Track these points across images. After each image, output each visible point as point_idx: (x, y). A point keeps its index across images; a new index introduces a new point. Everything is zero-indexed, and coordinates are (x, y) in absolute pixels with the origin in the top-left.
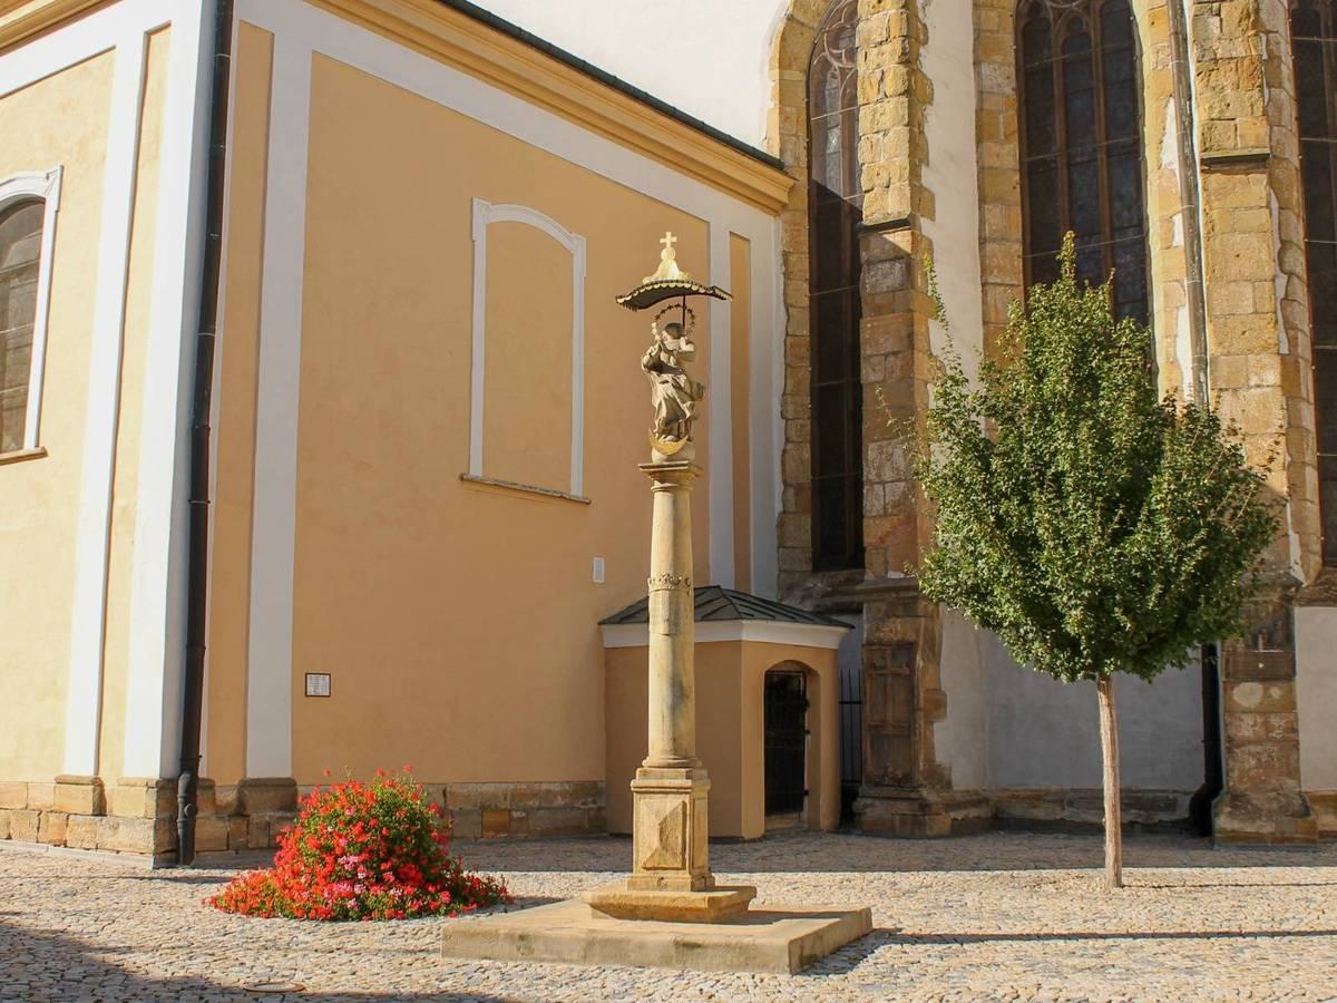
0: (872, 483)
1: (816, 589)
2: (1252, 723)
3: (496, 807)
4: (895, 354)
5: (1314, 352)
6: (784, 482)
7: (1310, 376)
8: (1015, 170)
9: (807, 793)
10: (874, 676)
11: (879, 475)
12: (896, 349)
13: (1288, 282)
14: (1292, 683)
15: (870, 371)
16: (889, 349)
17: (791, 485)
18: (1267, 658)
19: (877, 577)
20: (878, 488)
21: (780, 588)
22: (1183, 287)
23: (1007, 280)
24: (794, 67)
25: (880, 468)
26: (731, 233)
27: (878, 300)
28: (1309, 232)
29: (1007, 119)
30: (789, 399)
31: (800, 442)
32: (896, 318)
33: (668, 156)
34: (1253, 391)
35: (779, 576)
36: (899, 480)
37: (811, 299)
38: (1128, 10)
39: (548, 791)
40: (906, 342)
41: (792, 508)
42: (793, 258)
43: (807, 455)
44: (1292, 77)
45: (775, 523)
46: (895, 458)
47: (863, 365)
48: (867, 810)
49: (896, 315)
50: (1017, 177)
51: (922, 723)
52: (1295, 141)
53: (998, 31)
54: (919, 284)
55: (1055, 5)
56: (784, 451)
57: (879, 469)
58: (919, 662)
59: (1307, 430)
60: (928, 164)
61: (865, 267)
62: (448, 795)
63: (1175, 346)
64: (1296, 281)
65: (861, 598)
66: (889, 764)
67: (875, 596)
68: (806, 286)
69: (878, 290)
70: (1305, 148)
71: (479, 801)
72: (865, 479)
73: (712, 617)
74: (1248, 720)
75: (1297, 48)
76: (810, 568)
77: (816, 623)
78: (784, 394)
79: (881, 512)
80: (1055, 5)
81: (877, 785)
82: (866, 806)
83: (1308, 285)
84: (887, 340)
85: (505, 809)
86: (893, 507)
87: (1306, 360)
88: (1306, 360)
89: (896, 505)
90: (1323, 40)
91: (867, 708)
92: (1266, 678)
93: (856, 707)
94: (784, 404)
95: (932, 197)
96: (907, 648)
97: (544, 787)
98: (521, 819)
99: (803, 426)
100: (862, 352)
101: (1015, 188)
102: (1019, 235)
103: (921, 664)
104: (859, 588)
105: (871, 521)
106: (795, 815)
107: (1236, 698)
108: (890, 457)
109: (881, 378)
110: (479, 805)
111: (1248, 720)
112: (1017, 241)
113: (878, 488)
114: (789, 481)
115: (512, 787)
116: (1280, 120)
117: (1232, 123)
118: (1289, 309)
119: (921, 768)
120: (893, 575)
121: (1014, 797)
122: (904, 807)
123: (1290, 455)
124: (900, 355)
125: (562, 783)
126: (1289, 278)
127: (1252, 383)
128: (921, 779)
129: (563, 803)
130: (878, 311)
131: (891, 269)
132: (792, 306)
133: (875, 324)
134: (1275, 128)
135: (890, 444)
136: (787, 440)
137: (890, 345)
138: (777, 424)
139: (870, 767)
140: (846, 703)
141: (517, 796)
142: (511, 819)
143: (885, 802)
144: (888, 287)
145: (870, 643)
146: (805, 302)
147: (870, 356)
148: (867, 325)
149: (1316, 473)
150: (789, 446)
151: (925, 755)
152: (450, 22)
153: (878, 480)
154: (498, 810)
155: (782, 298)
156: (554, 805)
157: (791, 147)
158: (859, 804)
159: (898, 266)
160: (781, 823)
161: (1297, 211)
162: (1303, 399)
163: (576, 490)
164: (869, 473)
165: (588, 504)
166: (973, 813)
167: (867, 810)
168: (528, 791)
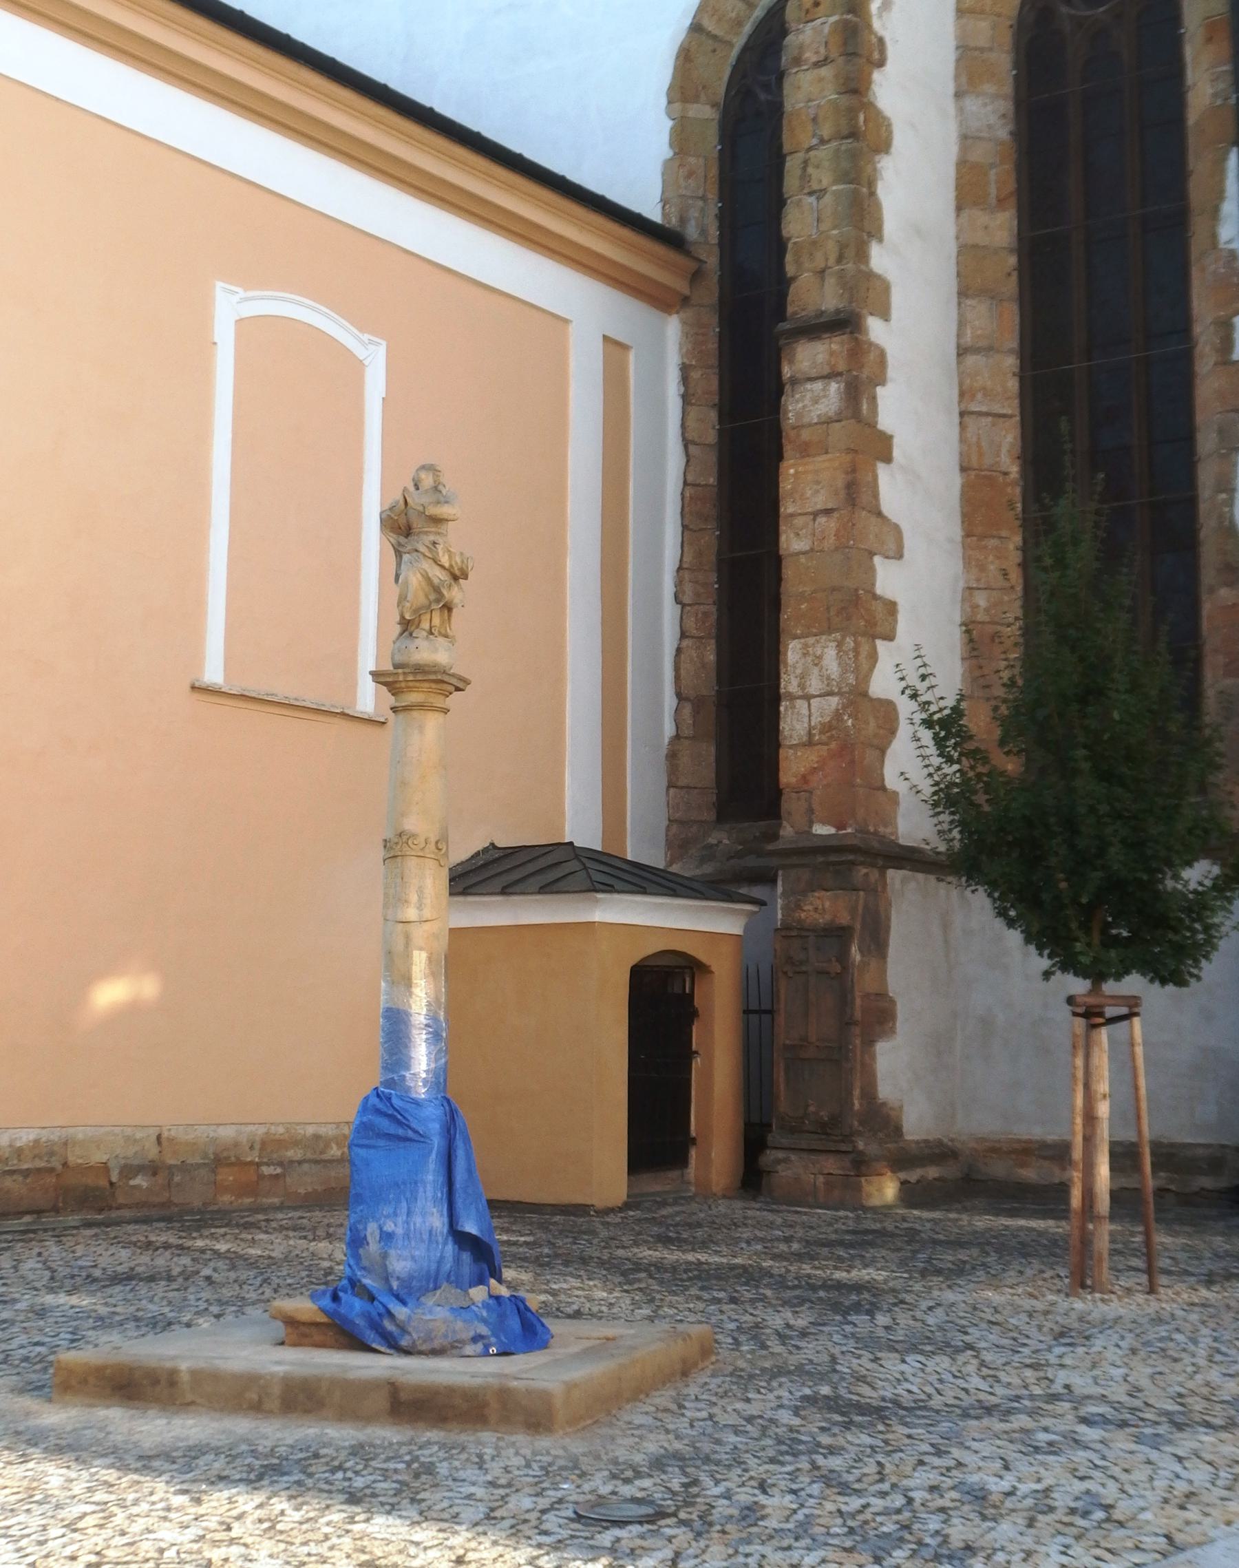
0: (792, 698)
1: (721, 847)
3: (238, 1159)
4: (827, 512)
6: (679, 695)
8: (1011, 251)
9: (693, 1141)
10: (790, 974)
11: (802, 686)
12: (829, 506)
15: (792, 535)
16: (819, 507)
17: (687, 699)
19: (797, 833)
20: (801, 705)
21: (669, 844)
23: (997, 409)
24: (703, 97)
25: (802, 677)
26: (606, 339)
27: (805, 435)
30: (687, 575)
31: (702, 638)
32: (829, 460)
33: (412, 178)
35: (668, 828)
36: (830, 694)
37: (721, 433)
38: (1175, 19)
39: (317, 1137)
40: (842, 494)
41: (687, 731)
43: (711, 657)
45: (665, 752)
46: (824, 663)
48: (779, 1168)
49: (829, 456)
50: (1013, 260)
51: (858, 1042)
53: (991, 49)
54: (865, 412)
55: (1073, 12)
56: (679, 651)
58: (855, 954)
60: (880, 240)
61: (788, 388)
62: (165, 1143)
65: (775, 862)
66: (811, 1102)
67: (795, 860)
68: (713, 415)
69: (806, 420)
71: (211, 1152)
72: (782, 691)
73: (555, 888)
77: (707, 899)
78: (680, 569)
79: (805, 739)
80: (1073, 12)
82: (779, 1161)
85: (251, 1163)
86: (821, 733)
89: (827, 728)
91: (781, 1019)
93: (766, 1018)
94: (679, 583)
95: (886, 288)
96: (838, 935)
97: (310, 1130)
98: (277, 1176)
99: (706, 614)
100: (782, 510)
102: (1015, 344)
103: (858, 958)
104: (770, 847)
105: (791, 751)
106: (674, 1174)
109: (808, 548)
110: (212, 1157)
112: (1011, 351)
113: (801, 705)
114: (684, 691)
115: (261, 1130)
119: (857, 1105)
120: (821, 829)
121: (994, 1150)
122: (831, 1165)
124: (836, 515)
125: (338, 1124)
128: (856, 1123)
129: (339, 1153)
130: (805, 451)
131: (824, 390)
133: (800, 469)
135: (818, 642)
136: (683, 635)
137: (820, 500)
138: (669, 613)
139: (784, 1105)
140: (766, 1012)
141: (268, 1144)
142: (261, 1177)
143: (805, 1155)
144: (819, 416)
145: (786, 927)
147: (792, 515)
148: (791, 471)
150: (686, 643)
151: (862, 1089)
152: (408, 136)
153: (800, 693)
154: (241, 1164)
156: (325, 1157)
157: (696, 215)
158: (770, 1156)
160: (655, 1184)
164: (789, 683)
165: (384, 723)
166: (932, 1172)
167: (779, 1168)
168: (286, 1136)
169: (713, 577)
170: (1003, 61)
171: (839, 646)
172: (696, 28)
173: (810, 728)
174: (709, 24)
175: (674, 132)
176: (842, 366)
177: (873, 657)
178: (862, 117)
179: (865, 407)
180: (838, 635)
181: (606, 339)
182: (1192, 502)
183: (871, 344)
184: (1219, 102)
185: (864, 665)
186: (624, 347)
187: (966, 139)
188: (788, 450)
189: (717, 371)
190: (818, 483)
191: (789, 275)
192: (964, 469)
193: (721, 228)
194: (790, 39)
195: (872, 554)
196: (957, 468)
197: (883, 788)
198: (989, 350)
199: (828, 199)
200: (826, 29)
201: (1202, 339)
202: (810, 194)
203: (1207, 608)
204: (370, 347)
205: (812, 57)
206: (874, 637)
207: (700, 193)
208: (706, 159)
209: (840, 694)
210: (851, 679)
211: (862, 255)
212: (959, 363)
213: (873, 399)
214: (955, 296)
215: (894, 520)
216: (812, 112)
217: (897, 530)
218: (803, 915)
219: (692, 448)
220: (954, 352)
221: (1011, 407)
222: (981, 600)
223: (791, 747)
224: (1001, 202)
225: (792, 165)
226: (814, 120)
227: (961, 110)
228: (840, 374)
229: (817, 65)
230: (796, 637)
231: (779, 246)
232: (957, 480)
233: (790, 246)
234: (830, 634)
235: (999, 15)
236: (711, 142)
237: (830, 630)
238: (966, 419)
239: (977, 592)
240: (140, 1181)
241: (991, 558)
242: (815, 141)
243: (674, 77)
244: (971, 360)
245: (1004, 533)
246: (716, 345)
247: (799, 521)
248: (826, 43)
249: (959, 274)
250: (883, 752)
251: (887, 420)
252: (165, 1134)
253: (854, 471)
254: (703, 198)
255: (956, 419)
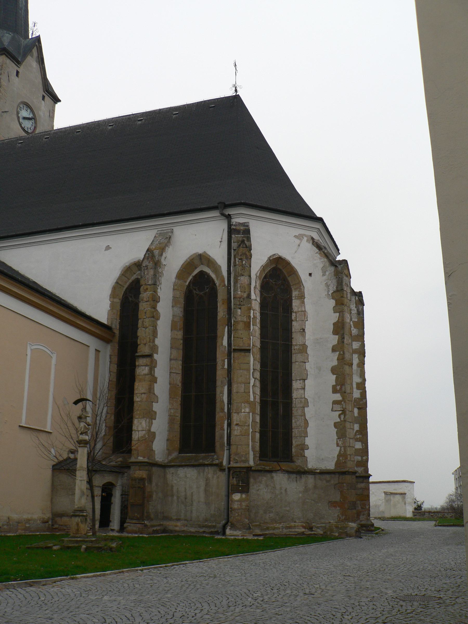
0: (135, 431)
2: (237, 504)
4: (144, 393)
5: (261, 400)
7: (259, 407)
8: (181, 339)
11: (137, 428)
13: (254, 381)
14: (249, 494)
16: (143, 392)
18: (241, 486)
20: (137, 432)
22: (226, 380)
26: (96, 350)
27: (140, 377)
28: (261, 366)
29: (180, 324)
34: (243, 413)
36: (143, 430)
37: (117, 370)
42: (112, 357)
44: (259, 323)
47: (135, 396)
50: (182, 342)
51: (146, 501)
52: (259, 340)
53: (180, 298)
57: (138, 426)
59: (257, 422)
60: (157, 338)
61: (137, 367)
63: (223, 397)
64: (257, 381)
68: (116, 366)
70: (262, 342)
72: (133, 429)
74: (236, 503)
75: (261, 314)
76: (111, 452)
81: (132, 519)
83: (260, 381)
84: (142, 389)
87: (258, 402)
88: (258, 402)
89: (142, 437)
90: (269, 312)
92: (241, 492)
96: (142, 479)
101: (181, 344)
102: (181, 359)
107: (233, 497)
108: (141, 423)
111: (236, 503)
116: (255, 335)
117: (242, 339)
118: (254, 388)
123: (252, 429)
124: (146, 394)
126: (255, 380)
127: (242, 411)
132: (112, 372)
133: (139, 384)
134: (254, 337)
137: (143, 391)
146: (115, 371)
147: (137, 393)
148: (137, 384)
149: (259, 434)
153: (137, 430)
155: (108, 369)
158: (125, 525)
159: (147, 368)
161: (258, 360)
162: (256, 414)
163: (48, 429)
164: (134, 428)
169: (114, 401)
170: (182, 300)
171: (145, 421)
172: (117, 283)
173: (139, 437)
174: (120, 283)
175: (110, 304)
176: (149, 364)
177: (152, 423)
178: (155, 313)
179: (153, 372)
180: (145, 419)
181: (96, 350)
182: (215, 394)
183: (155, 359)
184: (224, 317)
185: (151, 424)
186: (99, 351)
187: (174, 316)
188: (136, 380)
189: (117, 356)
190: (143, 387)
191: (138, 344)
192: (170, 384)
193: (120, 326)
194: (141, 295)
195: (153, 402)
196: (169, 384)
197: (152, 450)
198: (176, 360)
199: (147, 330)
200: (149, 294)
201: (218, 363)
202: (144, 328)
203: (217, 416)
204: (53, 354)
205: (145, 299)
206: (152, 419)
207: (116, 318)
208: (117, 311)
209: (145, 431)
210: (148, 428)
211: (154, 341)
212: (170, 362)
213: (154, 371)
214: (170, 348)
215: (157, 395)
216: (145, 311)
217: (157, 396)
218: (136, 475)
219: (111, 373)
220: (169, 360)
221: (180, 372)
222: (172, 411)
223: (134, 441)
224: (180, 329)
225: (140, 322)
226: (145, 313)
227: (173, 310)
228: (148, 365)
229: (146, 301)
230: (136, 418)
231: (137, 337)
232: (169, 386)
233: (139, 338)
234: (144, 418)
235: (181, 291)
236: (119, 307)
237: (144, 417)
238: (171, 374)
239: (171, 410)
240: (5, 527)
241: (174, 402)
242: (145, 317)
243: (111, 293)
244: (172, 361)
245: (177, 398)
246: (117, 351)
247: (138, 395)
248: (149, 297)
249: (171, 344)
250: (153, 442)
251: (156, 375)
252: (10, 517)
253: (150, 386)
254: (116, 319)
255: (169, 374)
